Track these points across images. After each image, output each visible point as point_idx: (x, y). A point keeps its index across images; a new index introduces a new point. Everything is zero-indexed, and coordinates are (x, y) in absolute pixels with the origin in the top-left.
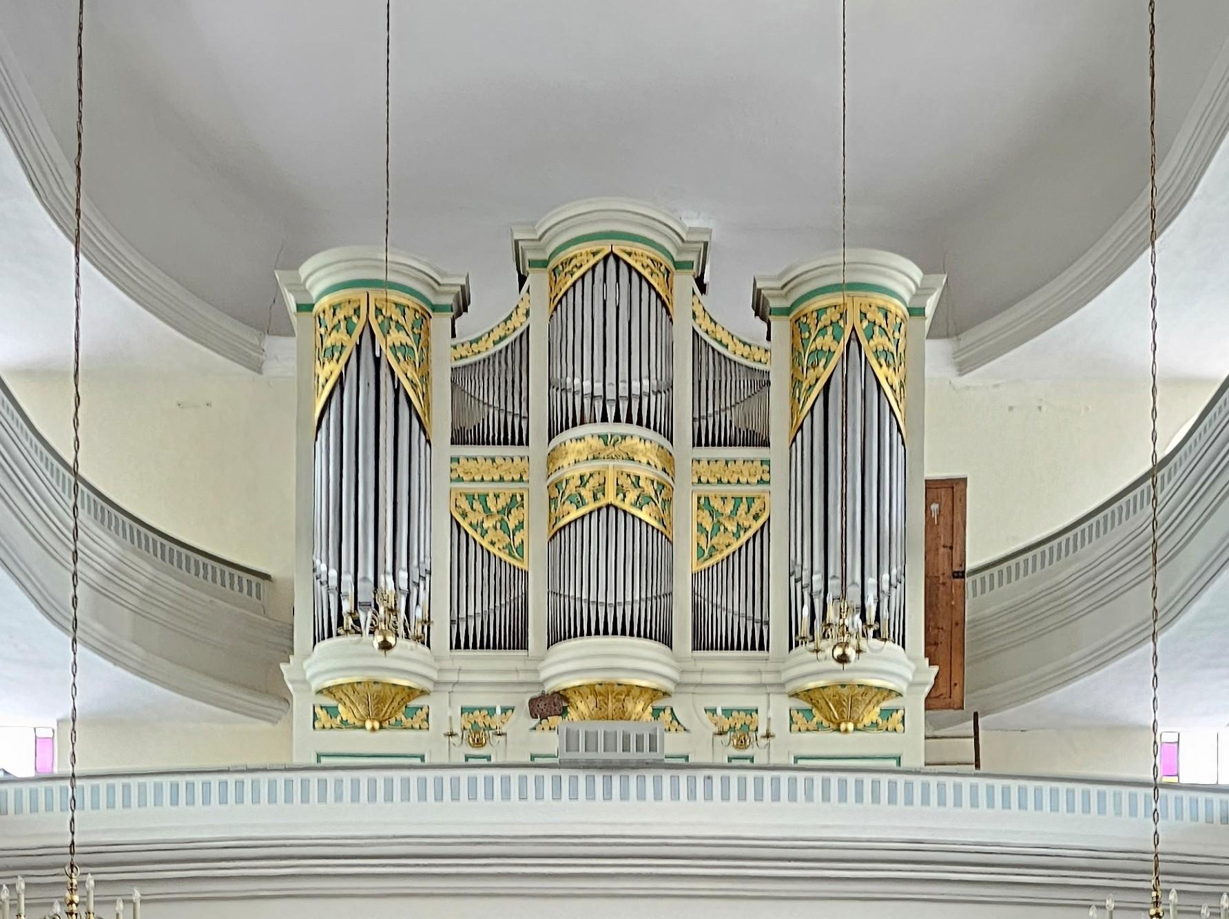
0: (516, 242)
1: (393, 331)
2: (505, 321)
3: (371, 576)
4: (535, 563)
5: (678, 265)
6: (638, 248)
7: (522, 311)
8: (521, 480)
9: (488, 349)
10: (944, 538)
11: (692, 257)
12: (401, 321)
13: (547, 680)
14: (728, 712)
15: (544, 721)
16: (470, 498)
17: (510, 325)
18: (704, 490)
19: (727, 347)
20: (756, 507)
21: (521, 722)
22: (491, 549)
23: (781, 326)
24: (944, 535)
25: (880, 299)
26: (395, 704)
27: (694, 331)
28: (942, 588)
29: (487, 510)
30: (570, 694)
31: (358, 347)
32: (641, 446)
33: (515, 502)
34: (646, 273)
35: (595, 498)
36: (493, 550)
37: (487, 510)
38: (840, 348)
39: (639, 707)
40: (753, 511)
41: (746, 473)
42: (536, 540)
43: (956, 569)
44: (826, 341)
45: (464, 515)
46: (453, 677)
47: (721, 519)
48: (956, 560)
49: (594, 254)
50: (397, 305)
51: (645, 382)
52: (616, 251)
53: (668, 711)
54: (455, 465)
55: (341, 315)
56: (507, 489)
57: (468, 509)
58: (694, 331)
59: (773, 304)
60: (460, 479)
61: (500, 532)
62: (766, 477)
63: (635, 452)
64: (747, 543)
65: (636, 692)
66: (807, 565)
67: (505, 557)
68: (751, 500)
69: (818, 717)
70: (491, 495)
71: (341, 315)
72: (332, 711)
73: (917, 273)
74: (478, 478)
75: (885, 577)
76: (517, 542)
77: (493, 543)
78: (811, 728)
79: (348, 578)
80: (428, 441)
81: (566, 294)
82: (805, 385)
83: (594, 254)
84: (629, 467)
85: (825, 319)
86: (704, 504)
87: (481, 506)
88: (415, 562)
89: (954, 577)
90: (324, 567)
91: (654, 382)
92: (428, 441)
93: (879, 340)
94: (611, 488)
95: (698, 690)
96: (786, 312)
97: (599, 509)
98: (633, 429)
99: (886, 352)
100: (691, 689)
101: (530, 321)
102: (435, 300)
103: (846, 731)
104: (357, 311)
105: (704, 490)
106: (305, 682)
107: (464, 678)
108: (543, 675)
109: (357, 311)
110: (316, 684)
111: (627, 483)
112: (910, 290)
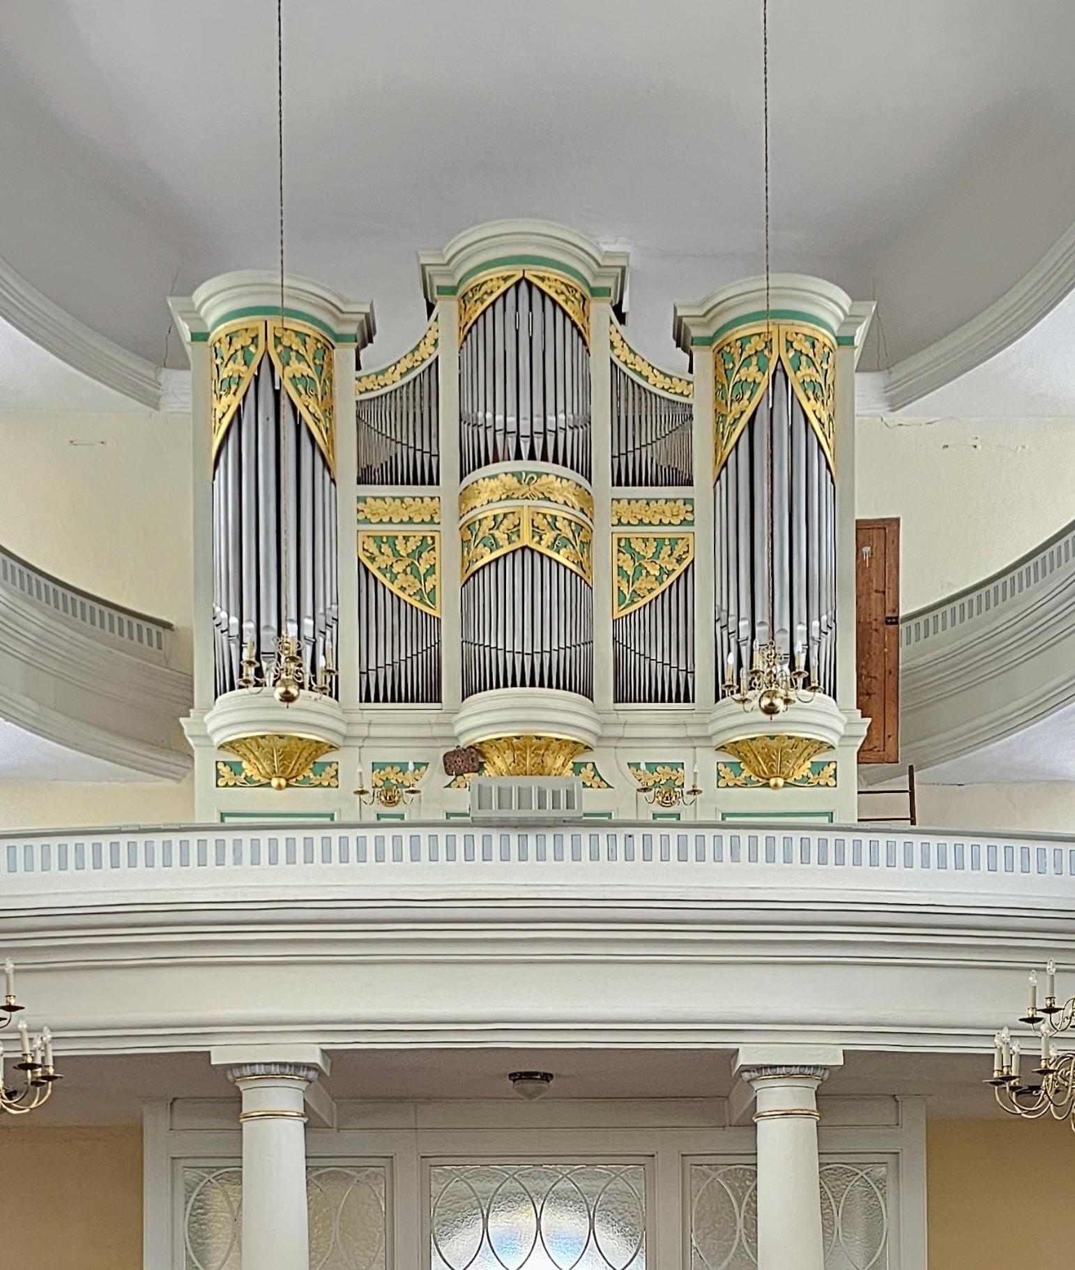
0: (423, 267)
2: (412, 352)
3: (274, 624)
4: (448, 611)
5: (595, 292)
6: (552, 273)
7: (430, 341)
8: (432, 521)
9: (395, 381)
11: (609, 283)
12: (302, 351)
13: (461, 734)
14: (651, 767)
15: (459, 778)
16: (378, 540)
17: (418, 356)
19: (646, 379)
23: (704, 357)
25: (807, 328)
26: (302, 760)
27: (612, 361)
28: (874, 634)
29: (395, 552)
30: (486, 748)
31: (257, 379)
32: (557, 484)
33: (426, 545)
34: (560, 299)
35: (510, 541)
36: (403, 596)
37: (395, 552)
38: (764, 381)
39: (559, 762)
40: (676, 554)
41: (668, 513)
42: (448, 585)
44: (751, 372)
46: (364, 731)
47: (642, 562)
48: (889, 606)
49: (505, 279)
51: (561, 416)
53: (590, 766)
54: (361, 506)
55: (237, 344)
57: (376, 552)
58: (612, 361)
59: (695, 332)
60: (367, 521)
61: (411, 578)
64: (670, 587)
65: (555, 745)
67: (416, 604)
68: (674, 542)
71: (237, 344)
72: (235, 768)
74: (386, 519)
75: (815, 624)
76: (429, 587)
77: (403, 589)
78: (739, 783)
79: (249, 626)
80: (333, 481)
81: (476, 322)
82: (729, 420)
85: (749, 349)
86: (624, 546)
88: (321, 610)
90: (224, 615)
91: (570, 416)
92: (333, 481)
93: (806, 371)
94: (526, 529)
95: (620, 744)
96: (708, 341)
97: (514, 552)
98: (548, 467)
100: (613, 743)
101: (439, 352)
102: (338, 330)
103: (776, 786)
104: (254, 340)
106: (207, 737)
107: (374, 732)
108: (458, 729)
109: (254, 340)
110: (218, 739)
112: (837, 318)
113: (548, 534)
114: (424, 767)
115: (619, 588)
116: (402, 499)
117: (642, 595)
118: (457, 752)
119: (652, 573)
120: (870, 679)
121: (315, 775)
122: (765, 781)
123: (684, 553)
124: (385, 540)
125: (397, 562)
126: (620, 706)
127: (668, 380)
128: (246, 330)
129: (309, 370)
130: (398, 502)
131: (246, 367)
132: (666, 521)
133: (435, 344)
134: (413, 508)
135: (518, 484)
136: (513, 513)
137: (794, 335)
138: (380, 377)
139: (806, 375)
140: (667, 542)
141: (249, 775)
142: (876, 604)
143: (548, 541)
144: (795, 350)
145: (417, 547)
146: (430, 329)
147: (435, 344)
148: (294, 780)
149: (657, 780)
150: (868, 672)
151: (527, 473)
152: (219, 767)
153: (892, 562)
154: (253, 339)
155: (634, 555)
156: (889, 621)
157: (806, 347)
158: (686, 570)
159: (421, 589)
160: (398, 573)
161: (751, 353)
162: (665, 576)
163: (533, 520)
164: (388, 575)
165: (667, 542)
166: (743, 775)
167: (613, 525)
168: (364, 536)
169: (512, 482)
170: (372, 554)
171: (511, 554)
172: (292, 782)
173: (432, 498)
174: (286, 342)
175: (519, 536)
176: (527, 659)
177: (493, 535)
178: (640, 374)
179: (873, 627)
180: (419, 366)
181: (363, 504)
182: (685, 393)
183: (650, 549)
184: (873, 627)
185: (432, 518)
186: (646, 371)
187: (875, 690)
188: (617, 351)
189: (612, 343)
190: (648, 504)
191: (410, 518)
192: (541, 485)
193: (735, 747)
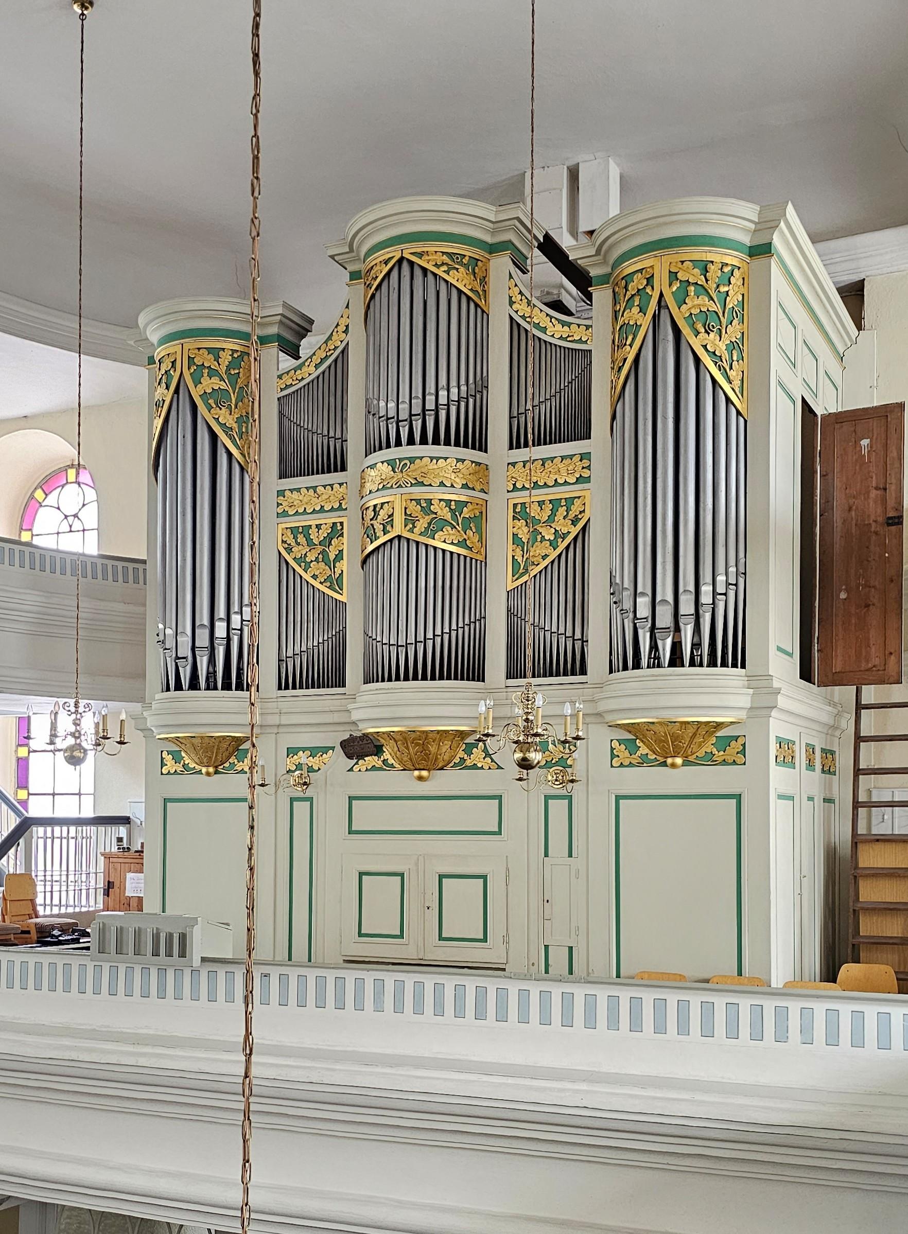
1: (205, 381)
2: (326, 342)
5: (493, 249)
6: (431, 247)
7: (342, 328)
8: (340, 508)
10: (877, 479)
15: (361, 762)
18: (521, 497)
20: (575, 509)
21: (338, 759)
22: (311, 581)
24: (876, 474)
27: (511, 318)
28: (874, 538)
33: (336, 531)
34: (440, 272)
35: (385, 532)
36: (316, 584)
38: (646, 322)
40: (572, 515)
41: (563, 472)
42: (348, 567)
43: (891, 514)
45: (289, 550)
48: (891, 503)
49: (386, 263)
50: (210, 350)
51: (443, 394)
52: (406, 255)
56: (328, 520)
57: (293, 544)
58: (511, 318)
60: (285, 514)
61: (322, 565)
62: (586, 473)
63: (424, 475)
64: (567, 548)
66: (628, 583)
68: (570, 501)
69: (644, 750)
70: (314, 527)
73: (749, 211)
74: (301, 510)
76: (338, 572)
77: (314, 577)
78: (634, 762)
83: (386, 263)
84: (418, 492)
86: (520, 513)
87: (305, 539)
88: (235, 607)
89: (889, 525)
93: (696, 303)
94: (399, 519)
96: (605, 279)
98: (430, 450)
99: (705, 314)
103: (673, 766)
105: (521, 497)
107: (285, 720)
108: (355, 716)
109: (174, 363)
111: (414, 508)
112: (744, 230)
113: (421, 521)
114: (331, 751)
115: (513, 557)
116: (314, 488)
117: (536, 563)
118: (352, 739)
119: (547, 538)
120: (867, 589)
121: (239, 762)
122: (662, 760)
123: (581, 512)
124: (301, 530)
125: (310, 551)
126: (511, 682)
127: (566, 328)
128: (168, 354)
129: (222, 383)
130: (311, 491)
131: (167, 390)
132: (560, 481)
133: (346, 331)
134: (324, 497)
135: (392, 473)
136: (388, 502)
137: (680, 264)
138: (298, 372)
139: (693, 306)
140: (563, 503)
141: (186, 763)
142: (875, 502)
143: (421, 528)
144: (681, 281)
145: (328, 534)
146: (342, 317)
147: (346, 331)
148: (222, 767)
149: (549, 760)
150: (866, 581)
151: (400, 460)
152: (164, 756)
153: (895, 454)
154: (173, 363)
155: (531, 521)
156: (890, 522)
157: (695, 275)
158: (584, 529)
159: (331, 575)
160: (312, 561)
161: (633, 293)
162: (560, 540)
163: (406, 508)
164: (303, 564)
165: (563, 503)
166: (639, 753)
167: (508, 491)
168: (283, 529)
169: (385, 469)
170: (289, 545)
171: (389, 543)
172: (220, 769)
173: (341, 484)
174: (198, 361)
175: (392, 526)
176: (402, 651)
177: (372, 525)
178: (537, 326)
179: (873, 529)
180: (332, 354)
181: (282, 498)
182: (584, 339)
183: (546, 513)
184: (873, 529)
185: (341, 504)
186: (545, 322)
187: (875, 601)
188: (515, 306)
189: (511, 297)
190: (543, 465)
191: (322, 506)
192: (413, 471)
193: (628, 728)
